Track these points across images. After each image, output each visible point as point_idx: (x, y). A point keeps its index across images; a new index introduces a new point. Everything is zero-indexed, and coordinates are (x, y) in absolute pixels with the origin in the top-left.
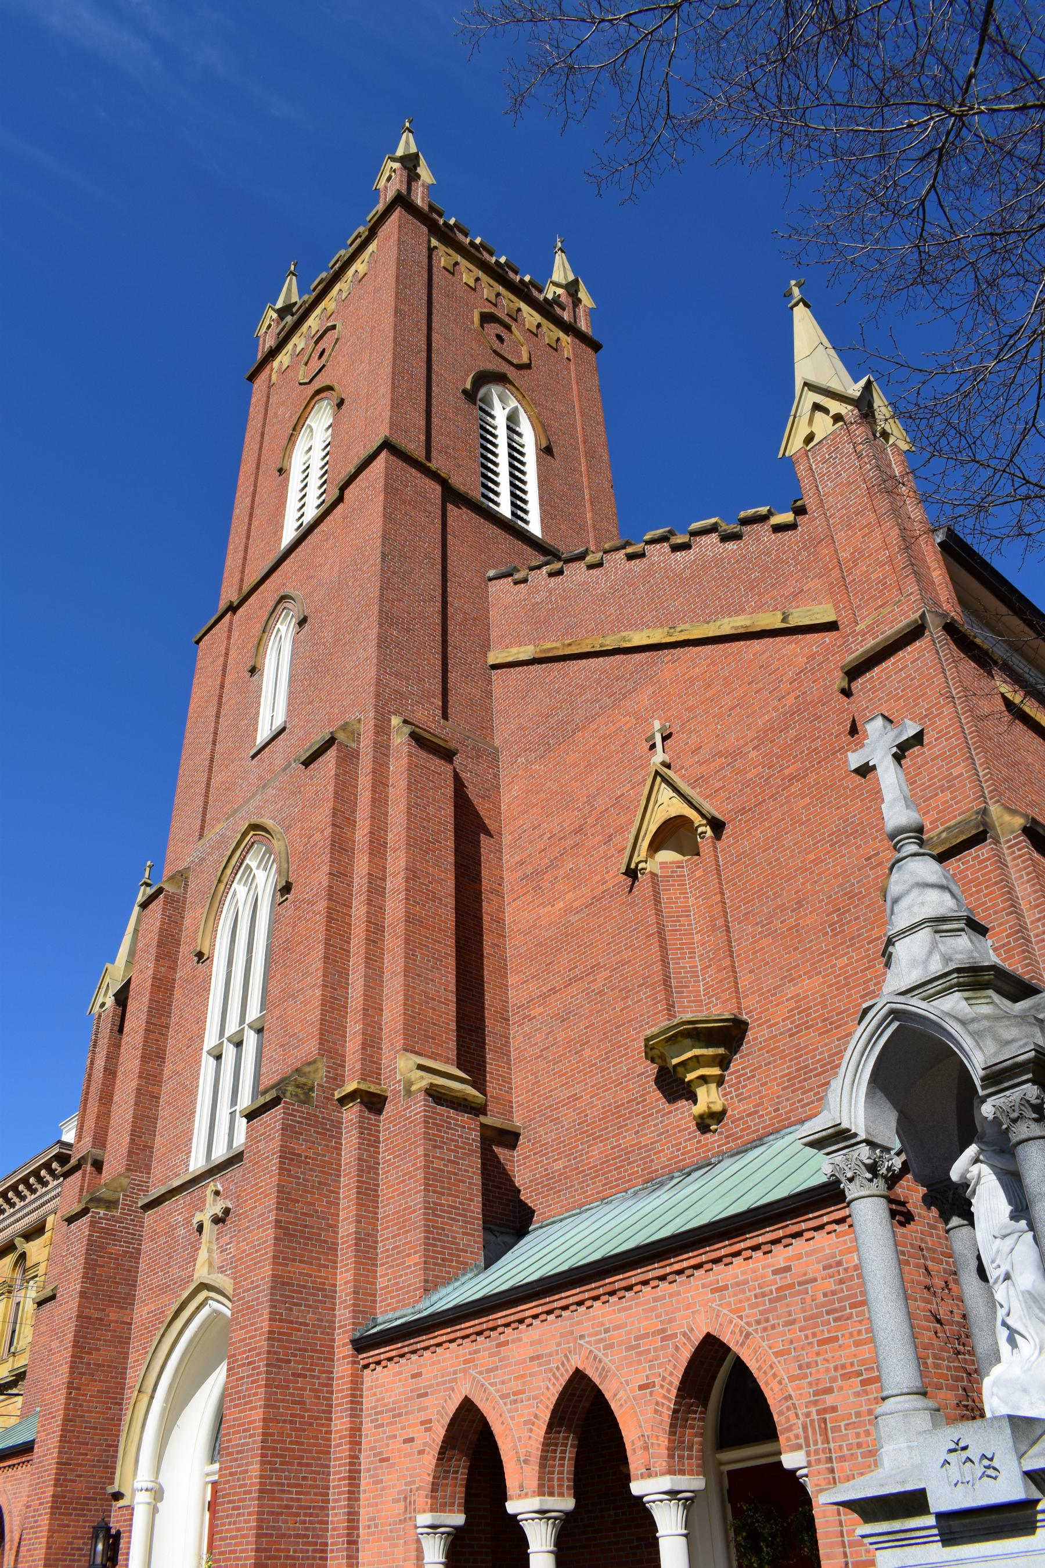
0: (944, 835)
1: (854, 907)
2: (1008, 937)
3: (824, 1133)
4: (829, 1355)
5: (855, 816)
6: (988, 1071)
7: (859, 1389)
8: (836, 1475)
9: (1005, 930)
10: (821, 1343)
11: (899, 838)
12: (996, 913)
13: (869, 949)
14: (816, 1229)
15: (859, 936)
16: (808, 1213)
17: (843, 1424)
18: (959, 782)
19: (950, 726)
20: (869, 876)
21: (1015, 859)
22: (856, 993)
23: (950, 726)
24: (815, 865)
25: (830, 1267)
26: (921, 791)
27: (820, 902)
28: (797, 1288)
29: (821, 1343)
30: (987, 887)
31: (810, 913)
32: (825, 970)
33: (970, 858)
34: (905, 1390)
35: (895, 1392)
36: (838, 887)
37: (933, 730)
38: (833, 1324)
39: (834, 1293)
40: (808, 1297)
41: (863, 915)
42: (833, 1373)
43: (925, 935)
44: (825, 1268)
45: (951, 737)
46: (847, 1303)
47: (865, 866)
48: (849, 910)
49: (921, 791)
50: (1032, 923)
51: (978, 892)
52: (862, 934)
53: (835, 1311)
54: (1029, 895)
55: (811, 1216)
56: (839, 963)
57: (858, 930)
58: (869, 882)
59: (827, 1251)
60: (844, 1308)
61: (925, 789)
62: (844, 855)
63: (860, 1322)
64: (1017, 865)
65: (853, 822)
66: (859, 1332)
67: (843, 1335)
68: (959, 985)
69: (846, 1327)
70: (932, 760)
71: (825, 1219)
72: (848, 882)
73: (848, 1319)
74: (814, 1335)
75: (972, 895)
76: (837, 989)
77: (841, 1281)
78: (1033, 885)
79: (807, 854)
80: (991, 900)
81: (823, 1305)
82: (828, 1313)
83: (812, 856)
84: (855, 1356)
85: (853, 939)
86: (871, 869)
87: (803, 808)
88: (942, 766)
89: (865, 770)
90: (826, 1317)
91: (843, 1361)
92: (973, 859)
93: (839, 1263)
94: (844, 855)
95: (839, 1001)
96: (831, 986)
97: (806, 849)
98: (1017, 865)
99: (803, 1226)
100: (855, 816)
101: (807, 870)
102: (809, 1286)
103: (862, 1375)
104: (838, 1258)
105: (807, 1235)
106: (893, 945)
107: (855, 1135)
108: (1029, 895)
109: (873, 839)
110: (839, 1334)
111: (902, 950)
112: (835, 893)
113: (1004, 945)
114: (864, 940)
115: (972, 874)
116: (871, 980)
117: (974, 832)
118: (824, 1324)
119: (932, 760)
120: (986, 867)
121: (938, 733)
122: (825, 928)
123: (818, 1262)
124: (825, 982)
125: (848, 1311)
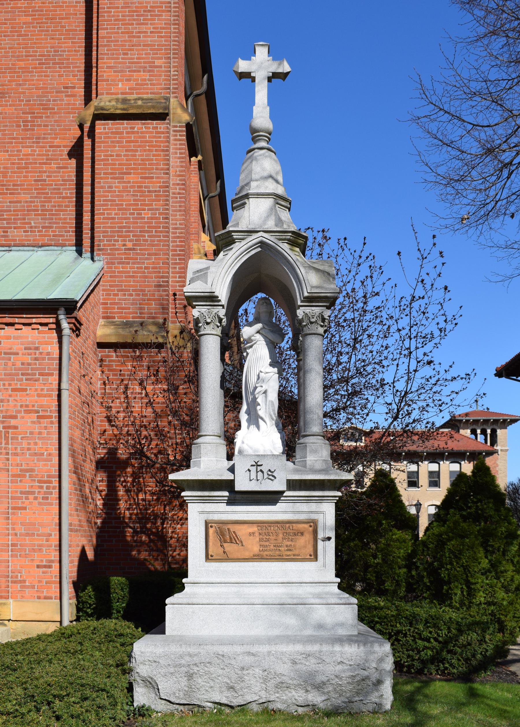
0: (140, 103)
1: (46, 117)
2: (160, 187)
3: (202, 294)
4: (18, 398)
5: (64, 51)
6: (310, 295)
7: (36, 420)
8: (10, 462)
9: (160, 182)
10: (13, 390)
11: (261, 133)
12: (157, 169)
13: (49, 151)
14: (24, 324)
15: (44, 138)
16: (23, 314)
17: (20, 436)
18: (158, 71)
19: (164, 28)
20: (63, 100)
21: (175, 140)
22: (31, 176)
23: (164, 28)
24: (23, 72)
25: (30, 349)
26: (129, 63)
27: (20, 101)
28: (3, 355)
29: (13, 390)
30: (156, 151)
31: (10, 105)
32: (11, 151)
33: (151, 126)
34: (216, 434)
35: (211, 434)
36: (37, 97)
37: (151, 24)
38: (24, 381)
39: (29, 364)
40: (10, 363)
41: (51, 125)
42: (19, 408)
43: (269, 202)
44: (26, 349)
45: (161, 37)
46: (20, 372)
47: (62, 92)
48: (41, 117)
49: (129, 63)
50: (173, 184)
51: (149, 150)
52: (47, 138)
53: (28, 374)
54: (177, 167)
55: (24, 316)
56: (24, 151)
57: (44, 134)
58: (62, 105)
59: (30, 340)
60: (35, 374)
61: (132, 63)
62: (48, 76)
63: (44, 384)
64: (176, 145)
65: (61, 55)
66: (42, 390)
67: (30, 389)
68: (288, 240)
69: (34, 385)
70: (144, 45)
71: (34, 321)
72: (45, 96)
73: (36, 381)
74: (10, 385)
75: (145, 151)
76: (18, 168)
77: (36, 359)
78: (182, 162)
79: (19, 60)
80: (156, 160)
81: (20, 369)
82: (23, 374)
83: (22, 64)
84: (37, 402)
85: (39, 138)
86: (66, 96)
87: (24, 23)
88: (149, 54)
89: (246, 76)
90: (20, 377)
91: (28, 403)
92: (154, 128)
93: (37, 348)
94: (48, 76)
95: (17, 177)
96: (13, 164)
97: (18, 56)
98: (176, 145)
99: (17, 320)
100: (64, 51)
101: (15, 72)
102: (12, 356)
103: (39, 413)
104: (37, 345)
105: (17, 326)
106: (248, 198)
107: (220, 301)
108: (177, 167)
109: (74, 76)
110: (28, 388)
111: (252, 203)
112: (34, 100)
113: (156, 191)
114: (47, 143)
115: (149, 137)
116: (45, 172)
117: (161, 111)
118: (18, 380)
119: (144, 45)
120: (160, 137)
121: (154, 28)
122: (19, 122)
123: (22, 344)
124: (10, 159)
125: (37, 376)
